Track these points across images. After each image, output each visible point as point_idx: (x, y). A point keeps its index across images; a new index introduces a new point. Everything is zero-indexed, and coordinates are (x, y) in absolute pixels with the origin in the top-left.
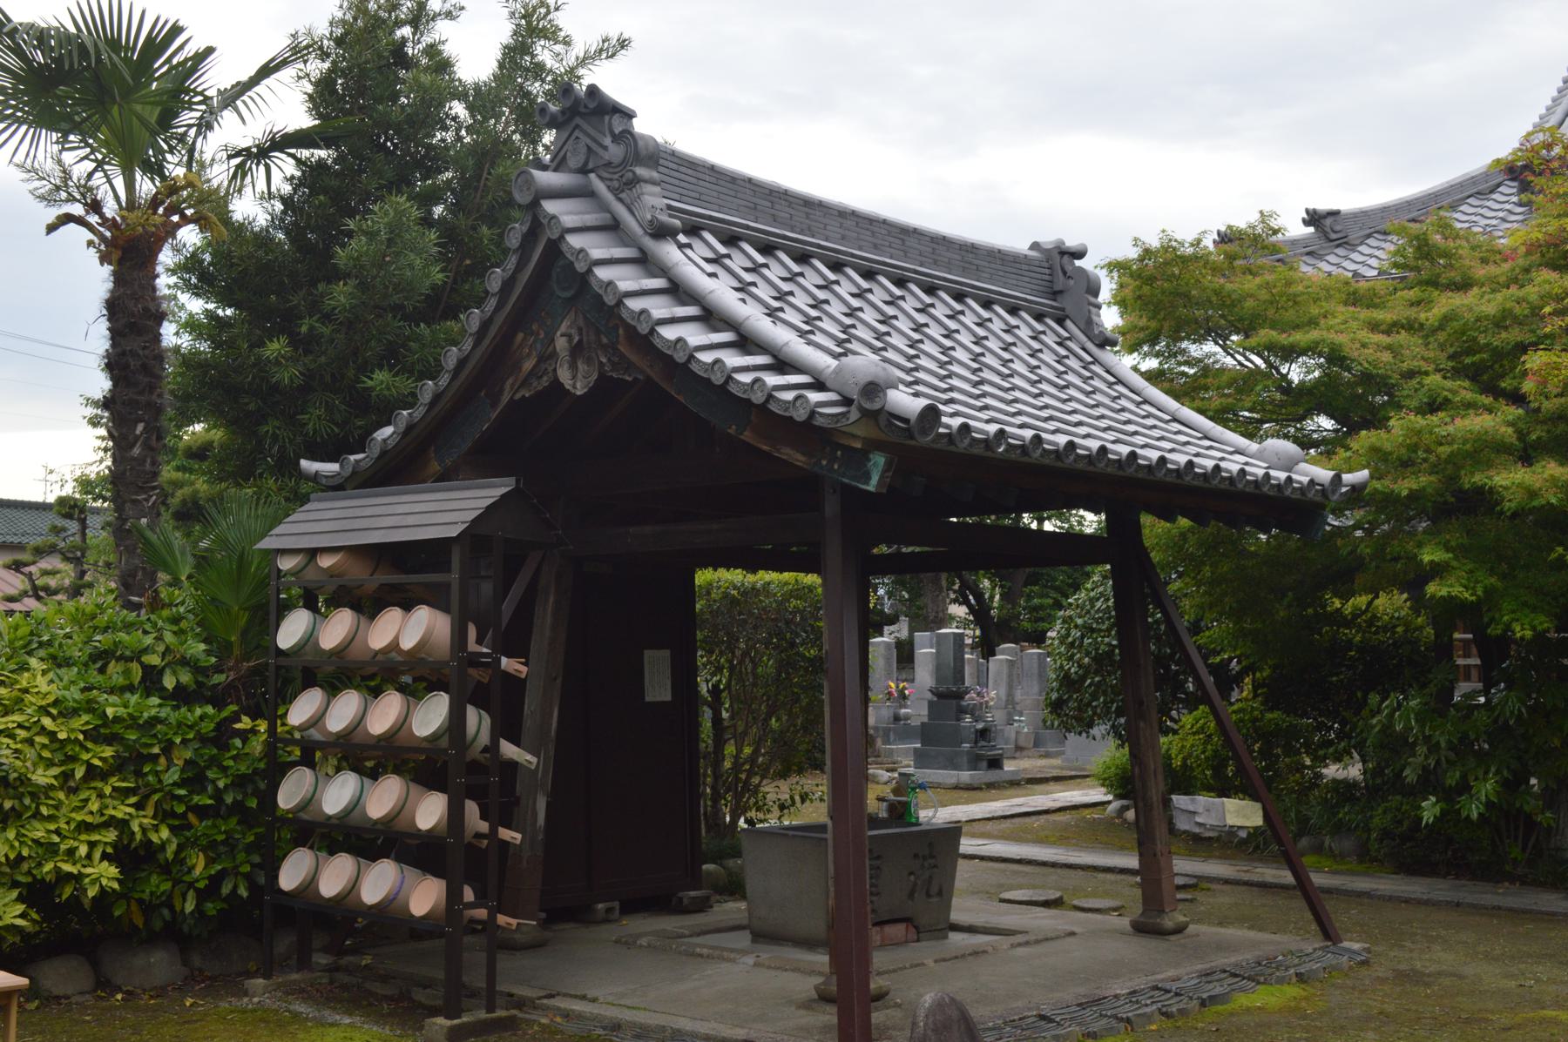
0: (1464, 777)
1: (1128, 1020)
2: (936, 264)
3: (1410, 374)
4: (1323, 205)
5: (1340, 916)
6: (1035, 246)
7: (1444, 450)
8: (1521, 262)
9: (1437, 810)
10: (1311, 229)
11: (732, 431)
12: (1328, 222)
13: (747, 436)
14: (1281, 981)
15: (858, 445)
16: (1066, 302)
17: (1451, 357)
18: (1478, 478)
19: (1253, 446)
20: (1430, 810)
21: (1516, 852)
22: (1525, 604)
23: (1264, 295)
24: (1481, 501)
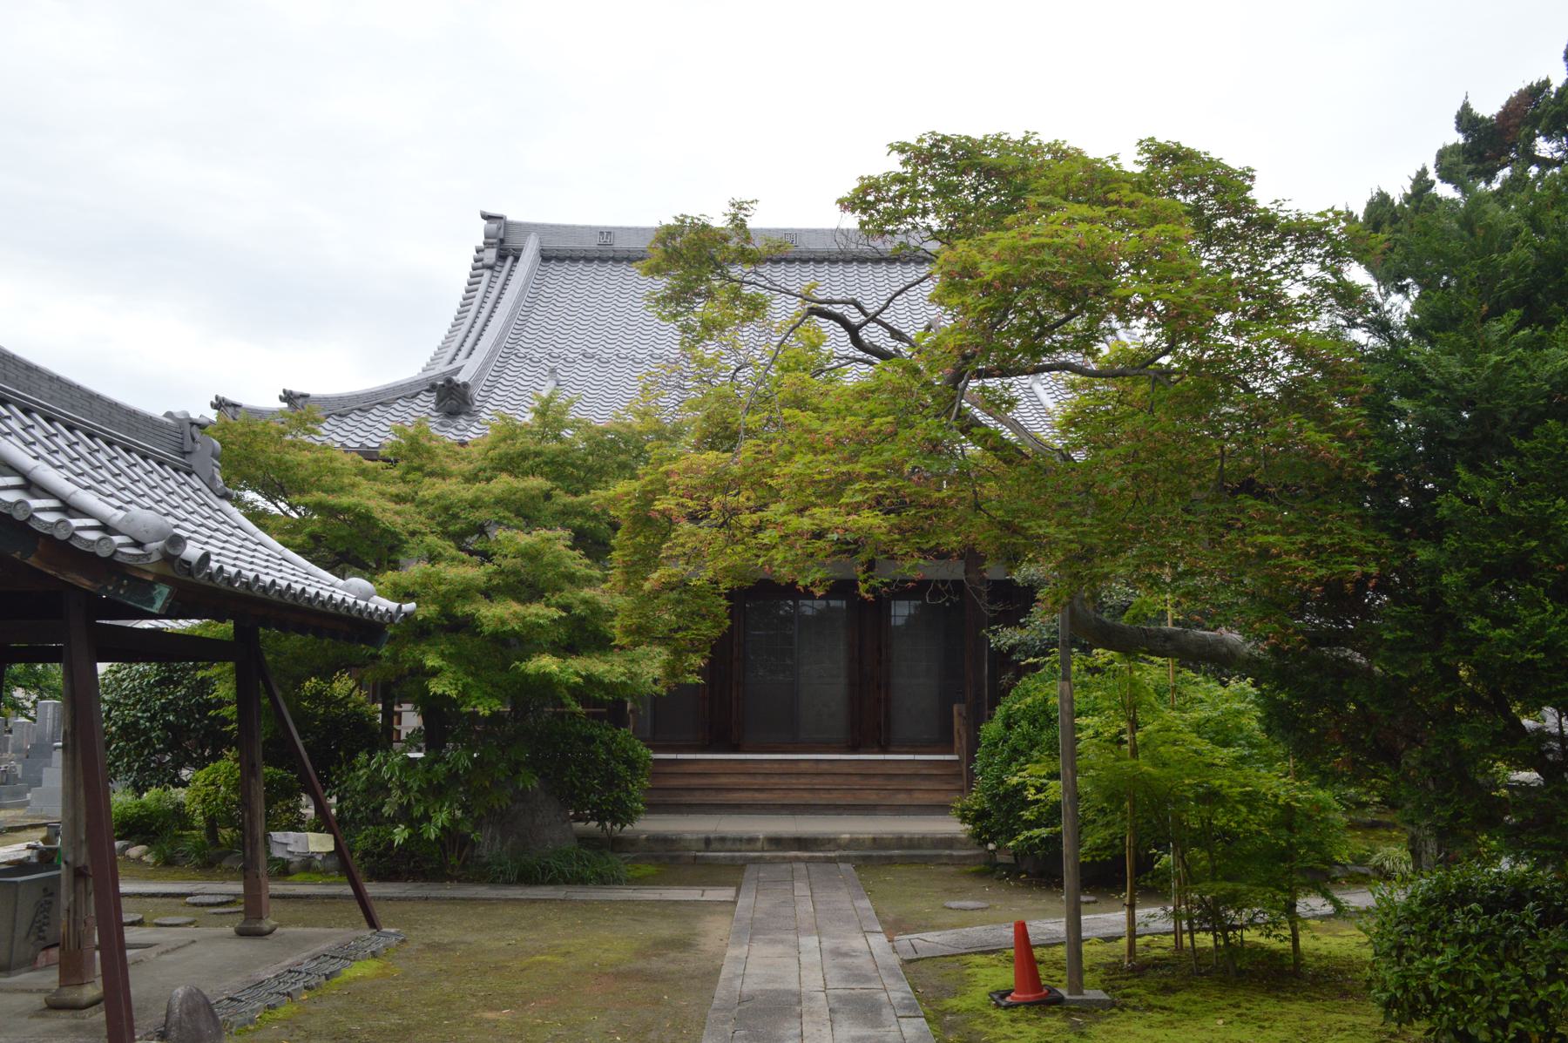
0: (426, 810)
1: (289, 994)
2: (111, 424)
3: (413, 534)
4: (298, 389)
5: (379, 911)
6: (169, 415)
7: (443, 588)
8: (478, 464)
9: (406, 834)
10: (285, 405)
11: (17, 555)
12: (300, 401)
13: (32, 561)
14: (364, 958)
15: (150, 578)
16: (194, 461)
17: (439, 524)
18: (468, 609)
19: (341, 582)
20: (400, 834)
21: (453, 860)
22: (485, 693)
23: (311, 466)
24: (467, 625)
